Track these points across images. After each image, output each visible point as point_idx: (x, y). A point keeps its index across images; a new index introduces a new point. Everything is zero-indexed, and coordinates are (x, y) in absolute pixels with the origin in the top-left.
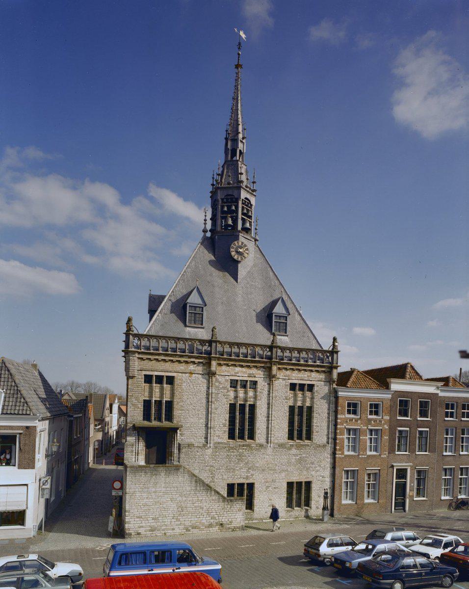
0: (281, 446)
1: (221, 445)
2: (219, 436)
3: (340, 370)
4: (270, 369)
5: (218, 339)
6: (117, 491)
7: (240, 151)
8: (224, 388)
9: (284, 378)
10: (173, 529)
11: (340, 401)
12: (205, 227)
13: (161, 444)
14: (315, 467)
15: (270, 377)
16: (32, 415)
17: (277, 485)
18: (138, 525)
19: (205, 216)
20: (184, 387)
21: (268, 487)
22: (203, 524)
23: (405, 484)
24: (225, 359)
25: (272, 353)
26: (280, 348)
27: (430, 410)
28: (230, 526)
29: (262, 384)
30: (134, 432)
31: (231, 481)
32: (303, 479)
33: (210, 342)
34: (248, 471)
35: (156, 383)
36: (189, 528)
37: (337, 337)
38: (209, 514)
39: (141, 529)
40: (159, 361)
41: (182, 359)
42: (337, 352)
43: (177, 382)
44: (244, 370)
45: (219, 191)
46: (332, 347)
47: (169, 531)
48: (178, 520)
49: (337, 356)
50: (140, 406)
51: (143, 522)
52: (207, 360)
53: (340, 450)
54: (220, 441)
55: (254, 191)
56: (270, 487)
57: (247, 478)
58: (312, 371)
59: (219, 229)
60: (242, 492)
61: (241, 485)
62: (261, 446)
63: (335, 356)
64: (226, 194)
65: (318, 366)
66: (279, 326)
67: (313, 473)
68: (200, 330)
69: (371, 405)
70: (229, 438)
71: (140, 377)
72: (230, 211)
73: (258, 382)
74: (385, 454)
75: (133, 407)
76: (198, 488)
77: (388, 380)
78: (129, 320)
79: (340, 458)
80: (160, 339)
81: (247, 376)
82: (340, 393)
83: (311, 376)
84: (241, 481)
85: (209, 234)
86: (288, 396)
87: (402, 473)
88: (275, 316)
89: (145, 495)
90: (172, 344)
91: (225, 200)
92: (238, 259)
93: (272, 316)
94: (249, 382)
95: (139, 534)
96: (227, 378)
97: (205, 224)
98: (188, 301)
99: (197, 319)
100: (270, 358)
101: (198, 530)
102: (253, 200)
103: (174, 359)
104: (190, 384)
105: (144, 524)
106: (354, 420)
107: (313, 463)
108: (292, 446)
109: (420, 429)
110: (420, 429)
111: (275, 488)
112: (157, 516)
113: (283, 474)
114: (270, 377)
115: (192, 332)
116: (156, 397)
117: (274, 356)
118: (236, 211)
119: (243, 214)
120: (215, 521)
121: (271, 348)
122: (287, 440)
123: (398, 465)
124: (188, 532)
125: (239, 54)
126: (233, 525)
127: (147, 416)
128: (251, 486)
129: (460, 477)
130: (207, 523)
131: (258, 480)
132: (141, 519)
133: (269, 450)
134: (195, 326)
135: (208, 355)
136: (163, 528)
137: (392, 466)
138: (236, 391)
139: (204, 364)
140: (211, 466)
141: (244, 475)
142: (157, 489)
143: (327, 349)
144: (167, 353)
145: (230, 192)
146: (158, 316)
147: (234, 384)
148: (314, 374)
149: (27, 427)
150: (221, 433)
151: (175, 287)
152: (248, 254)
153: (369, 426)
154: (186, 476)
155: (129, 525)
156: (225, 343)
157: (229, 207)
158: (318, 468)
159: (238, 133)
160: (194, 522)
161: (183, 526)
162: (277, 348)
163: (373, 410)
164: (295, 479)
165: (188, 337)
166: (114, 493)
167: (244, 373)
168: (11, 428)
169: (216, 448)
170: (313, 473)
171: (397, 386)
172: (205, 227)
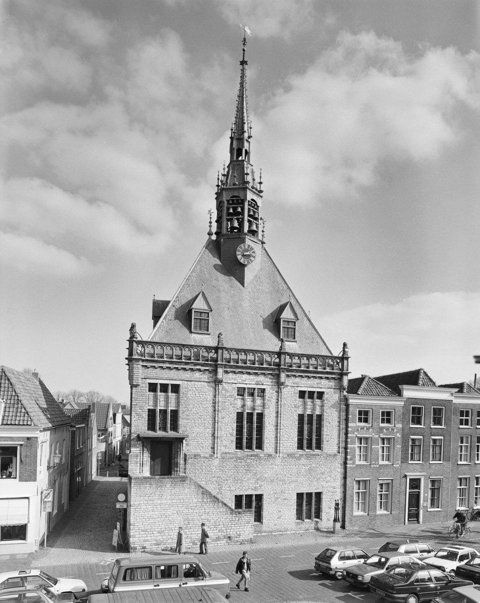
0: (291, 455)
1: (228, 455)
3: (351, 376)
4: (278, 376)
5: (225, 346)
7: (246, 150)
8: (231, 396)
9: (293, 385)
11: (351, 409)
12: (210, 230)
15: (279, 384)
17: (286, 496)
19: (211, 218)
21: (277, 498)
24: (231, 367)
26: (288, 354)
29: (270, 393)
32: (313, 490)
33: (216, 349)
34: (256, 482)
37: (347, 342)
40: (164, 369)
41: (187, 367)
42: (347, 358)
43: (182, 390)
44: (252, 377)
46: (342, 353)
50: (144, 415)
52: (213, 366)
57: (255, 489)
58: (321, 378)
59: (224, 231)
60: (251, 504)
62: (270, 456)
63: (345, 362)
65: (328, 373)
67: (324, 483)
70: (237, 448)
71: (144, 385)
72: (236, 213)
73: (266, 389)
74: (398, 464)
76: (205, 500)
77: (400, 387)
78: (133, 326)
80: (165, 346)
81: (253, 383)
85: (214, 237)
87: (415, 484)
90: (177, 351)
91: (231, 202)
96: (234, 386)
97: (210, 226)
100: (278, 365)
104: (196, 389)
105: (149, 538)
109: (412, 437)
113: (293, 485)
114: (279, 384)
116: (161, 406)
117: (282, 363)
118: (242, 213)
119: (249, 216)
121: (279, 354)
124: (195, 546)
127: (152, 426)
128: (259, 498)
135: (214, 362)
138: (243, 399)
139: (210, 372)
147: (241, 392)
149: (28, 439)
153: (381, 434)
156: (232, 349)
158: (329, 479)
164: (305, 490)
166: (118, 506)
168: (11, 439)
170: (324, 483)
171: (409, 392)
172: (210, 230)
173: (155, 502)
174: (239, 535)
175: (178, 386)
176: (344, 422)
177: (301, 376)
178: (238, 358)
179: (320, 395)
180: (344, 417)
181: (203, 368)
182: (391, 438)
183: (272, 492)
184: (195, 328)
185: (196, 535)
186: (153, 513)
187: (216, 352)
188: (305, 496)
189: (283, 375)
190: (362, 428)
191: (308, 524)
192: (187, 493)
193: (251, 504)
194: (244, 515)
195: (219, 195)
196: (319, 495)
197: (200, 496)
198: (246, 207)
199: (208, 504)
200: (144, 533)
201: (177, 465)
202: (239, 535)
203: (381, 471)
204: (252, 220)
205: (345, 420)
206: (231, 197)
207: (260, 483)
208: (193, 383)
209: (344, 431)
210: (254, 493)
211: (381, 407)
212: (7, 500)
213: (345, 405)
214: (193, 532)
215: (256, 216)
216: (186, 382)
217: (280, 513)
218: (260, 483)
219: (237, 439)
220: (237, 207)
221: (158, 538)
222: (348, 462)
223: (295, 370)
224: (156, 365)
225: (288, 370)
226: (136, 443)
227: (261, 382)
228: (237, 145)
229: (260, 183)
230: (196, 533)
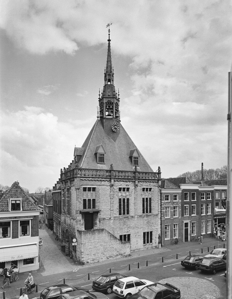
1: (116, 218)
2: (115, 214)
5: (114, 170)
6: (75, 243)
8: (116, 192)
10: (102, 259)
11: (163, 195)
12: (98, 115)
13: (90, 219)
16: (37, 210)
17: (139, 234)
20: (100, 192)
23: (188, 229)
24: (116, 179)
25: (135, 175)
26: (138, 172)
27: (188, 197)
28: (125, 255)
31: (121, 234)
32: (149, 231)
33: (110, 171)
39: (89, 260)
40: (96, 181)
41: (99, 179)
42: (160, 173)
44: (124, 183)
45: (104, 99)
46: (158, 171)
47: (100, 260)
48: (104, 254)
49: (161, 175)
50: (82, 202)
53: (163, 216)
54: (116, 216)
58: (151, 182)
60: (125, 239)
61: (125, 236)
64: (107, 100)
65: (153, 180)
66: (135, 162)
67: (153, 227)
68: (103, 165)
69: (166, 196)
71: (81, 189)
74: (180, 217)
76: (111, 239)
77: (180, 185)
79: (163, 220)
81: (125, 185)
86: (142, 194)
87: (186, 225)
89: (90, 244)
90: (94, 173)
91: (107, 103)
92: (115, 131)
93: (97, 154)
95: (88, 262)
98: (133, 155)
99: (102, 160)
100: (110, 176)
101: (112, 258)
103: (96, 179)
105: (90, 258)
107: (153, 223)
108: (144, 216)
109: (192, 205)
110: (192, 205)
111: (139, 236)
113: (142, 229)
114: (136, 186)
115: (100, 166)
117: (136, 176)
118: (112, 109)
119: (116, 110)
121: (134, 173)
122: (142, 214)
123: (185, 222)
124: (108, 260)
126: (126, 254)
127: (85, 207)
128: (129, 235)
129: (208, 224)
131: (132, 232)
132: (89, 255)
133: (136, 219)
134: (101, 163)
135: (111, 175)
136: (98, 258)
137: (183, 222)
140: (113, 228)
141: (126, 231)
142: (95, 241)
143: (155, 172)
144: (128, 178)
146: (85, 159)
147: (120, 189)
148: (151, 184)
149: (35, 216)
151: (89, 145)
152: (119, 128)
153: (174, 205)
154: (106, 233)
155: (84, 259)
156: (116, 171)
157: (109, 106)
158: (155, 225)
160: (110, 254)
163: (167, 198)
164: (146, 231)
165: (99, 169)
166: (73, 244)
168: (27, 217)
169: (115, 219)
170: (153, 227)
171: (184, 187)
173: (91, 241)
174: (125, 253)
175: (95, 188)
177: (143, 182)
178: (125, 175)
179: (128, 189)
180: (160, 198)
181: (105, 180)
182: (177, 206)
183: (134, 233)
184: (99, 161)
186: (91, 246)
187: (135, 174)
188: (146, 233)
189: (137, 182)
190: (167, 203)
191: (148, 245)
192: (104, 236)
193: (125, 239)
194: (126, 244)
195: (100, 100)
196: (151, 232)
197: (109, 237)
198: (114, 106)
199: (112, 241)
200: (87, 256)
201: (96, 224)
202: (125, 253)
203: (174, 220)
207: (129, 229)
208: (101, 186)
209: (160, 204)
210: (127, 234)
211: (173, 193)
212: (27, 246)
213: (160, 193)
214: (107, 254)
215: (118, 110)
216: (98, 186)
217: (137, 242)
218: (129, 229)
219: (119, 210)
220: (110, 106)
223: (127, 178)
224: (86, 179)
225: (139, 179)
227: (128, 185)
228: (108, 78)
229: (119, 95)
230: (108, 253)
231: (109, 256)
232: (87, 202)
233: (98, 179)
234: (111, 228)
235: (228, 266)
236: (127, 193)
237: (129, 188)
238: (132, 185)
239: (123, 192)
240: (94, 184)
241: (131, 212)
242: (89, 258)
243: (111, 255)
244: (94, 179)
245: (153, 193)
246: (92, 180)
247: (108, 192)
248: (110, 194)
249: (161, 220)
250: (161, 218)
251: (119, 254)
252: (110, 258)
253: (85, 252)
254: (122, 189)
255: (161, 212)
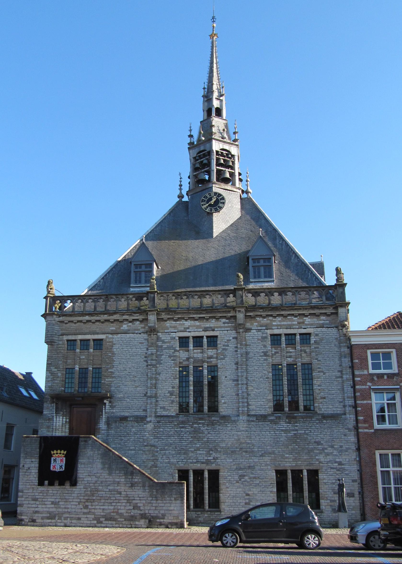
0: (263, 418)
12: (181, 192)
14: (323, 449)
18: (33, 509)
19: (181, 181)
22: (121, 515)
28: (162, 520)
30: (52, 405)
31: (182, 466)
35: (393, 466)
36: (101, 519)
37: (340, 267)
38: (131, 501)
39: (37, 515)
43: (105, 345)
44: (197, 323)
50: (60, 375)
51: (39, 506)
53: (365, 421)
55: (235, 140)
56: (244, 476)
57: (208, 462)
75: (52, 377)
82: (352, 340)
83: (303, 323)
84: (198, 466)
88: (252, 259)
94: (205, 337)
96: (173, 335)
97: (181, 189)
101: (114, 522)
102: (234, 150)
106: (385, 377)
111: (255, 478)
112: (57, 500)
113: (267, 459)
120: (139, 512)
125: (213, 27)
130: (127, 514)
132: (37, 503)
140: (152, 446)
145: (202, 148)
147: (183, 342)
148: (307, 320)
150: (166, 403)
158: (329, 450)
159: (212, 92)
160: (108, 511)
161: (93, 516)
162: (242, 290)
164: (289, 464)
167: (198, 327)
172: (181, 192)
176: (349, 370)
185: (101, 511)
200: (33, 502)
204: (224, 169)
205: (350, 367)
206: (198, 154)
210: (206, 468)
213: (348, 348)
216: (110, 336)
221: (51, 510)
222: (360, 425)
226: (50, 405)
227: (210, 327)
229: (235, 133)
230: (102, 507)
231: (103, 516)
232: (90, 375)
233: (109, 318)
234: (146, 446)
235: (219, 500)
236: (211, 352)
237: (216, 337)
238: (227, 329)
239: (180, 349)
240: (98, 330)
241: (225, 403)
242: (36, 509)
243: (112, 514)
244: (98, 318)
245: (315, 348)
246: (90, 321)
247: (142, 350)
248: (146, 353)
249: (358, 435)
250: (357, 428)
251: (141, 515)
252: (107, 522)
253: (27, 491)
254: (191, 340)
255: (355, 406)
